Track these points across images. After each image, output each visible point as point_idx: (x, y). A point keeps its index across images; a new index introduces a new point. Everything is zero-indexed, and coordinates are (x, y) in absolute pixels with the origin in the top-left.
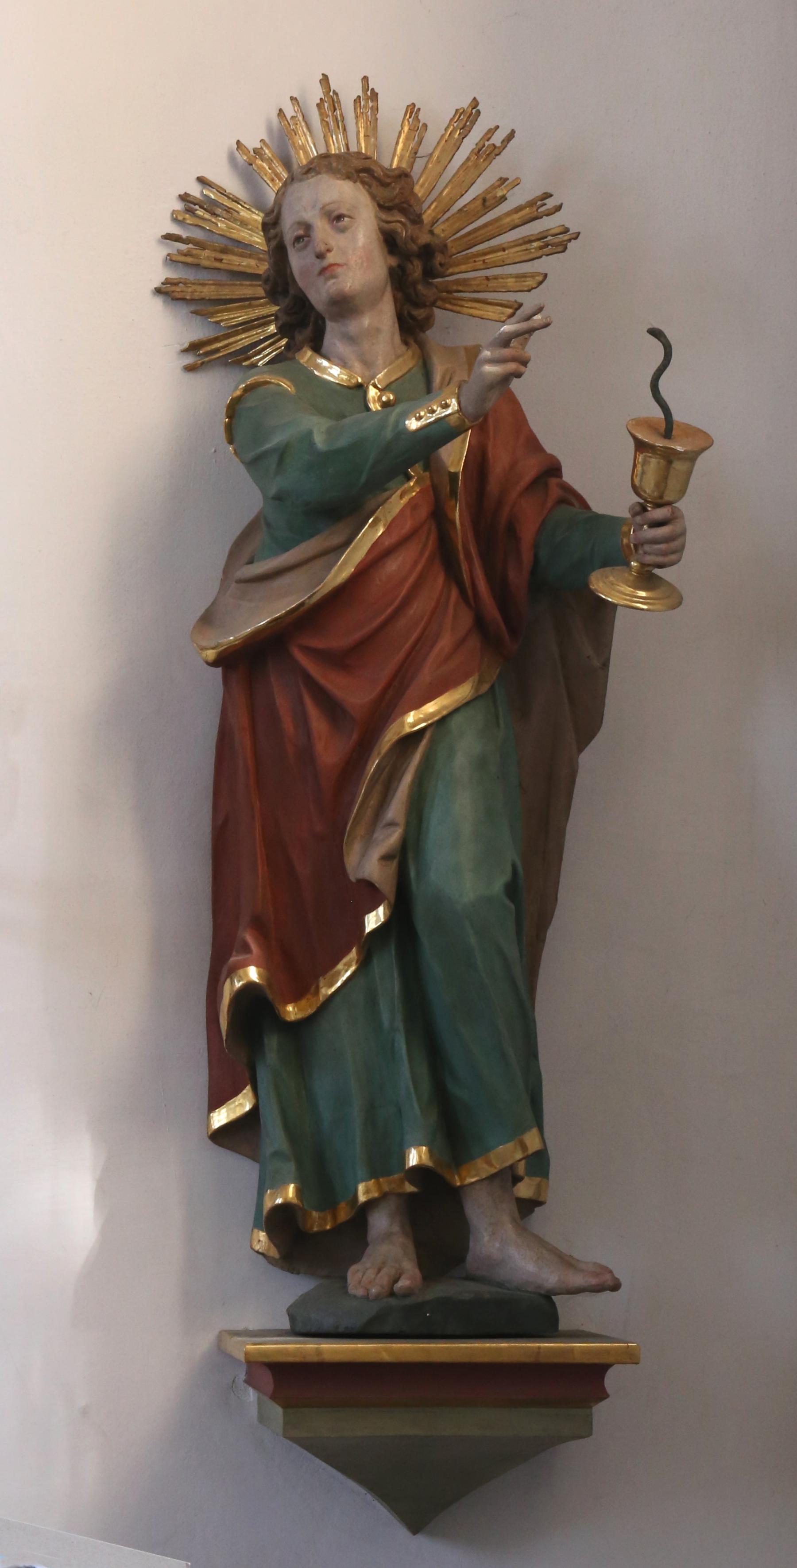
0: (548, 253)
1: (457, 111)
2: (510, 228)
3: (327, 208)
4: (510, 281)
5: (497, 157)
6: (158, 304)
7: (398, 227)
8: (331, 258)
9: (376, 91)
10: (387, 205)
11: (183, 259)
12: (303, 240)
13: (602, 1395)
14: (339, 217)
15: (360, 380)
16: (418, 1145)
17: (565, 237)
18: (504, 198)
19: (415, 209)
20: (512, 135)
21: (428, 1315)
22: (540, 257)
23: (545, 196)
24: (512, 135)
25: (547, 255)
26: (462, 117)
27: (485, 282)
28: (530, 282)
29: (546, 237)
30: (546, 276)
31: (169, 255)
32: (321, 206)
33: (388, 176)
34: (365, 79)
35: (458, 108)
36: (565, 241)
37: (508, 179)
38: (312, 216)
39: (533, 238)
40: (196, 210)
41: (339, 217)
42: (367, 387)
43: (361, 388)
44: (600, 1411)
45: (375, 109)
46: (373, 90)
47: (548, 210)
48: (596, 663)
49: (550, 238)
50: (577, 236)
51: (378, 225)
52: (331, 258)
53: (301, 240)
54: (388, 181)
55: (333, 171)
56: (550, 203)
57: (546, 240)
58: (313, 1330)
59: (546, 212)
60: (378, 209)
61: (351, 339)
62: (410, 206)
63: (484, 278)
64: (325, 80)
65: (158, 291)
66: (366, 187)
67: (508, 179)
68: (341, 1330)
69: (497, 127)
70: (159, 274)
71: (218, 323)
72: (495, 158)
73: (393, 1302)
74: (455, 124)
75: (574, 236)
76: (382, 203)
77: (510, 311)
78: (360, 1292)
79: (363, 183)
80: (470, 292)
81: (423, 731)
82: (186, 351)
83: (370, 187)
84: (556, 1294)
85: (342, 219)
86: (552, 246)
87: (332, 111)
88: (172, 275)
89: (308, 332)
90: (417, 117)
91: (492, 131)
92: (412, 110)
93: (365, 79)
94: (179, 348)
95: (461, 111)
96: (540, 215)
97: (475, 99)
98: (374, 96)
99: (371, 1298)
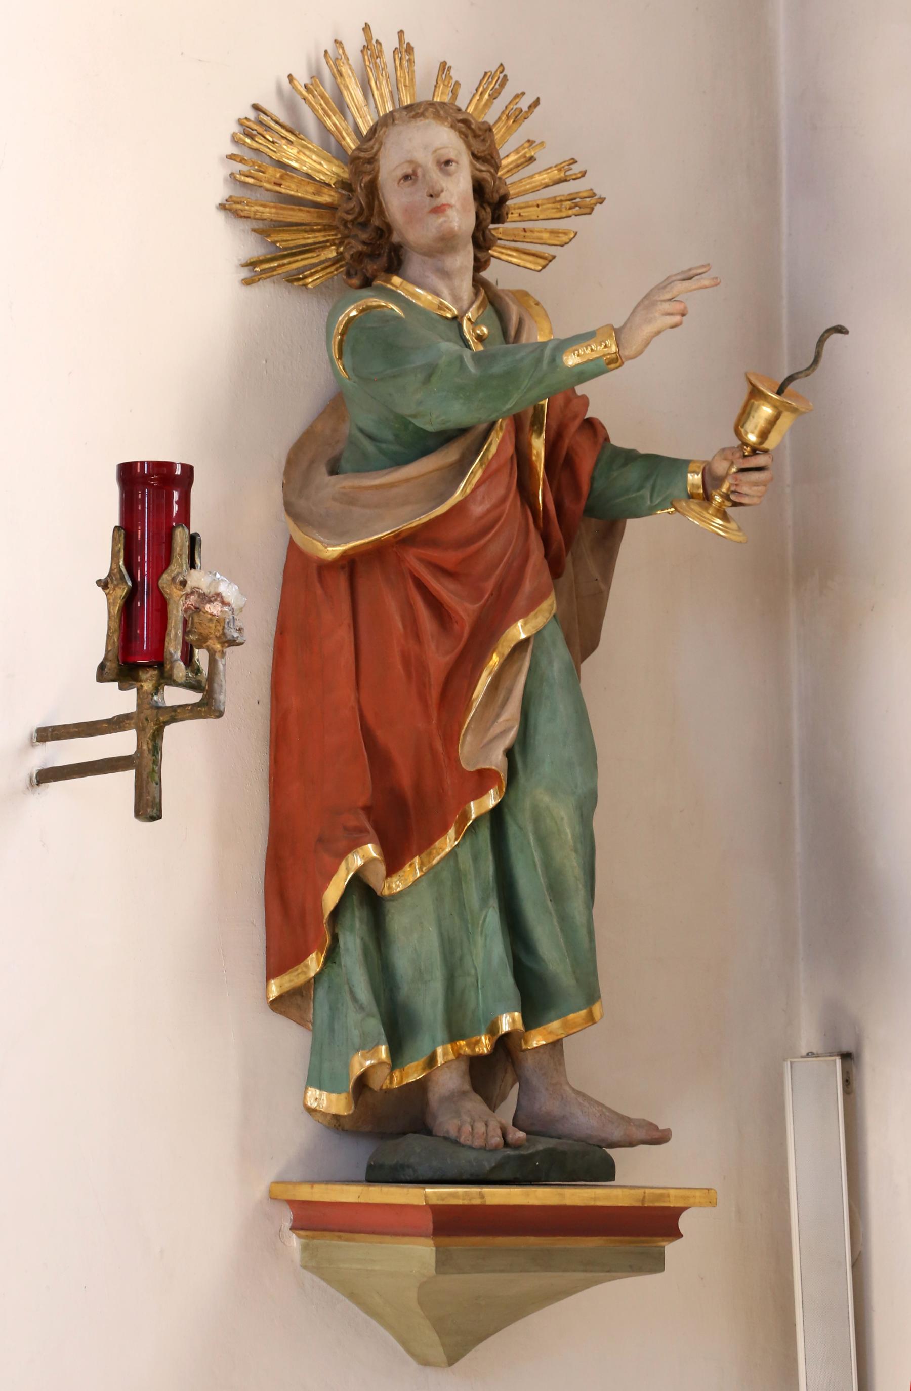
0: (577, 214)
1: (486, 74)
2: (542, 187)
3: (439, 152)
4: (545, 236)
5: (526, 120)
6: (220, 218)
7: (486, 176)
8: (443, 199)
9: (412, 44)
10: (479, 155)
11: (243, 178)
12: (411, 178)
13: (676, 1234)
14: (448, 162)
15: (456, 312)
16: (509, 1010)
17: (593, 201)
18: (531, 159)
19: (497, 161)
20: (537, 102)
21: (537, 1164)
22: (570, 216)
23: (572, 161)
24: (537, 102)
25: (576, 215)
26: (490, 80)
27: (523, 233)
28: (565, 239)
29: (575, 199)
30: (576, 234)
31: (232, 174)
32: (434, 149)
33: (480, 129)
34: (401, 33)
35: (487, 71)
36: (592, 204)
37: (535, 142)
38: (427, 160)
39: (563, 198)
40: (255, 135)
41: (448, 162)
42: (462, 320)
43: (456, 320)
44: (672, 1249)
45: (410, 61)
46: (408, 44)
47: (575, 174)
48: (603, 586)
49: (578, 200)
50: (601, 201)
51: (472, 172)
52: (443, 199)
53: (409, 178)
54: (480, 133)
55: (437, 116)
56: (576, 169)
57: (574, 201)
58: (436, 1177)
59: (574, 177)
60: (471, 158)
61: (445, 274)
62: (492, 158)
63: (522, 229)
64: (367, 29)
65: (222, 207)
66: (462, 136)
67: (535, 142)
68: (464, 1177)
69: (523, 93)
70: (220, 191)
71: (274, 243)
72: (524, 121)
73: (510, 1152)
74: (485, 86)
75: (600, 201)
76: (476, 153)
77: (542, 262)
78: (478, 1143)
79: (461, 132)
80: (507, 241)
81: (527, 641)
82: (243, 266)
83: (466, 136)
84: (613, 1145)
85: (451, 164)
86: (580, 208)
87: (374, 58)
88: (239, 193)
89: (384, 260)
90: (449, 74)
91: (517, 96)
92: (444, 67)
93: (401, 33)
94: (237, 263)
95: (489, 74)
96: (568, 179)
97: (501, 65)
98: (410, 49)
99: (487, 1149)
